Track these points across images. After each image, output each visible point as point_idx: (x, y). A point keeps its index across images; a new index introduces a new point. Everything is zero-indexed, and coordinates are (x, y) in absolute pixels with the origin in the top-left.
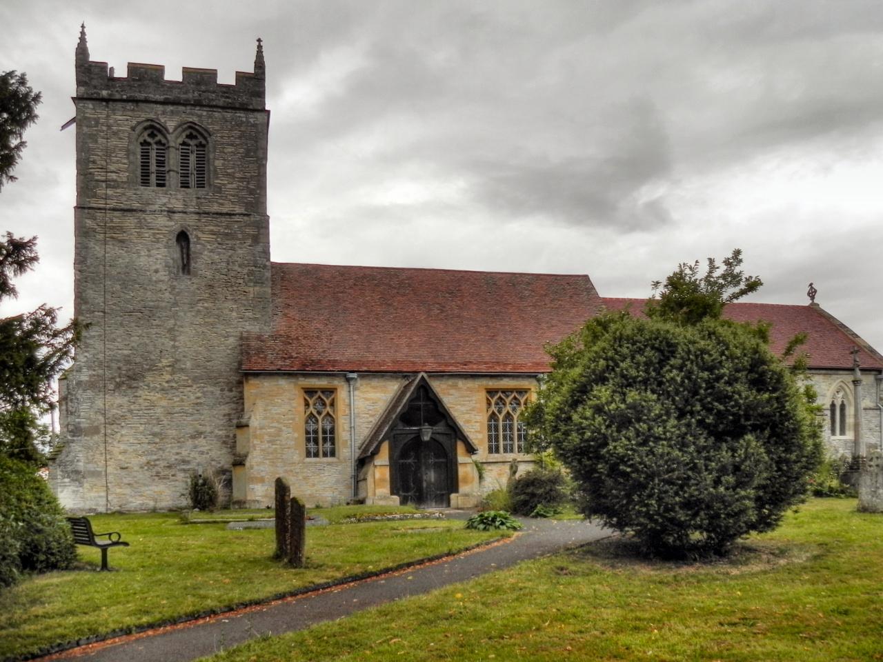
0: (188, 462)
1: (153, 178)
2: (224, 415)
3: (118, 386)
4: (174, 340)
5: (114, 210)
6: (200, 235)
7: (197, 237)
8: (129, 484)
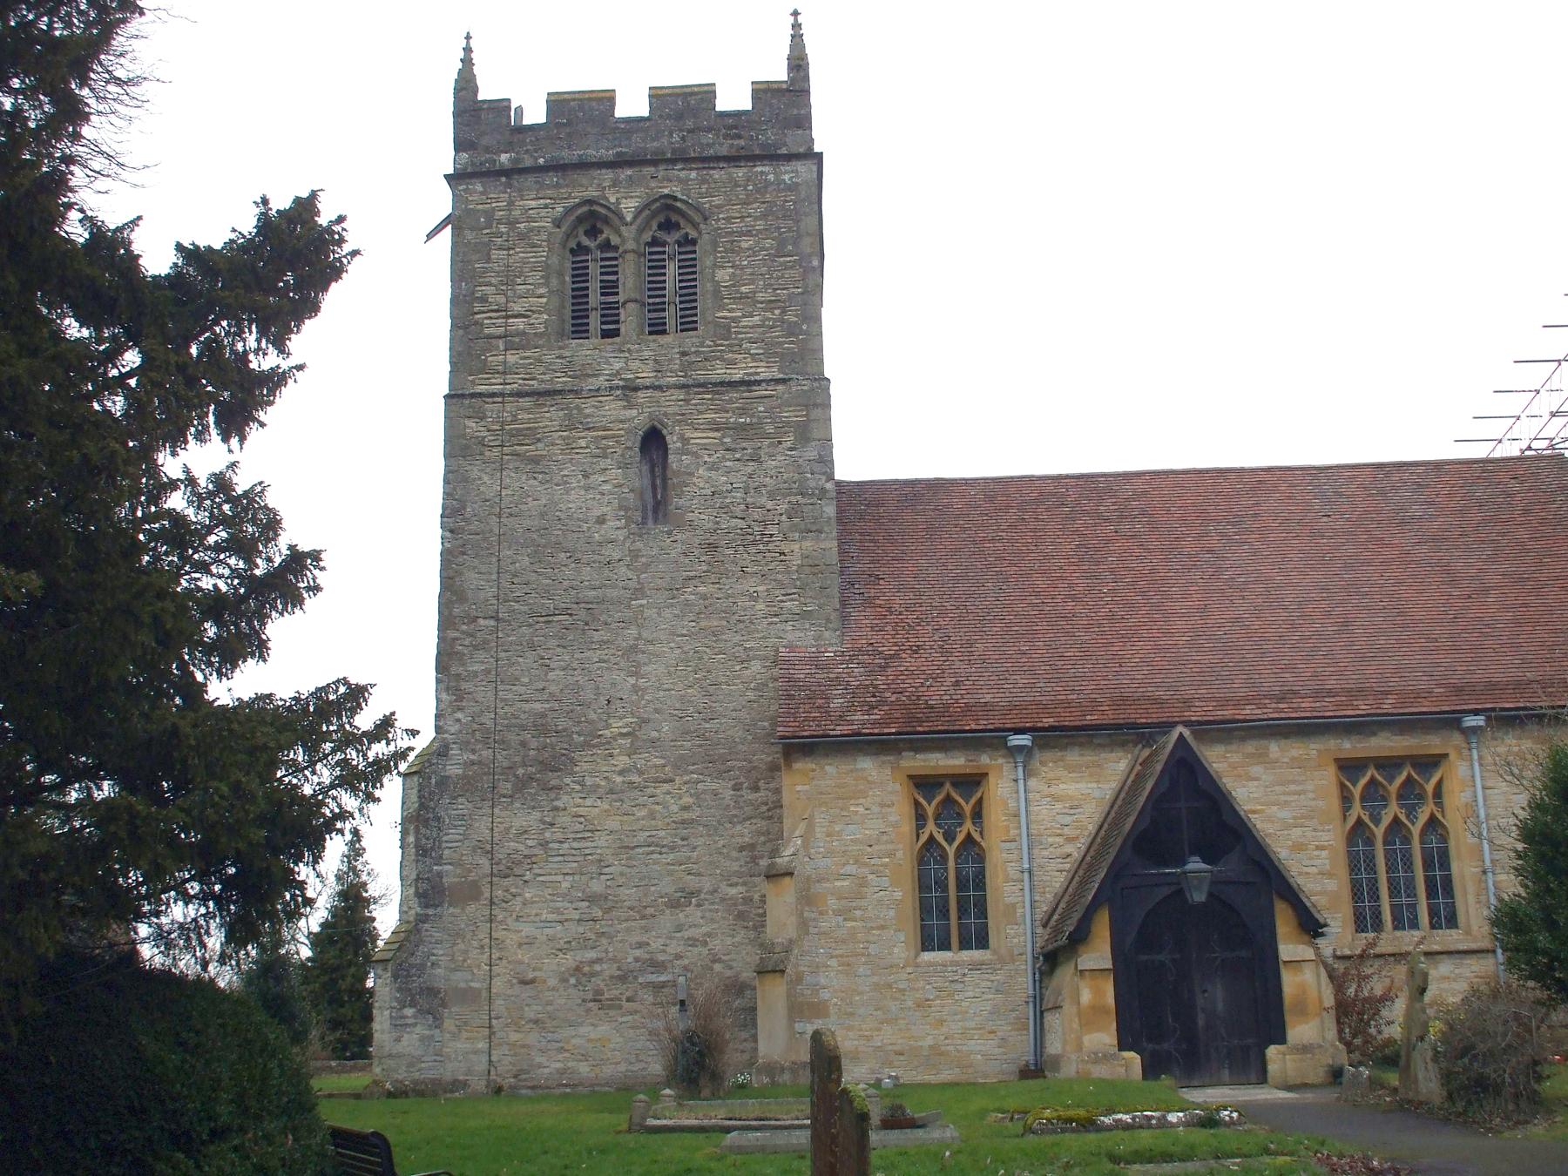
0: (657, 966)
1: (594, 321)
2: (741, 849)
3: (522, 784)
8: (536, 1022)
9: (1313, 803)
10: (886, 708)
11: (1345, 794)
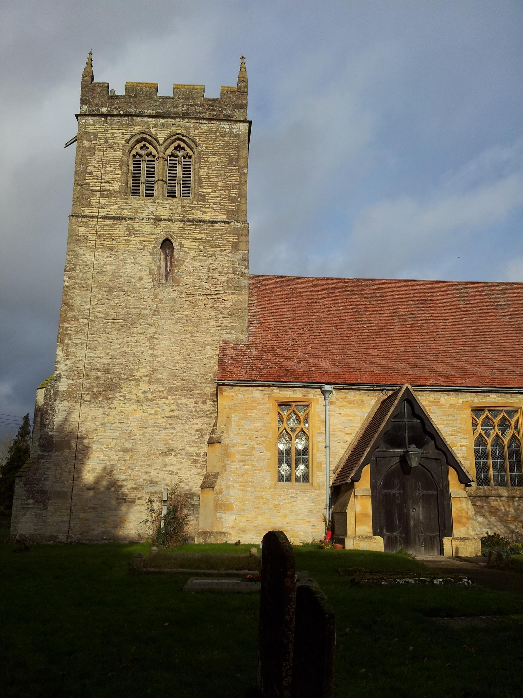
0: (153, 483)
1: (143, 188)
2: (197, 431)
3: (95, 396)
4: (153, 349)
5: (106, 218)
6: (184, 242)
7: (180, 244)
8: (93, 508)
9: (460, 425)
10: (267, 370)
11: (474, 422)
